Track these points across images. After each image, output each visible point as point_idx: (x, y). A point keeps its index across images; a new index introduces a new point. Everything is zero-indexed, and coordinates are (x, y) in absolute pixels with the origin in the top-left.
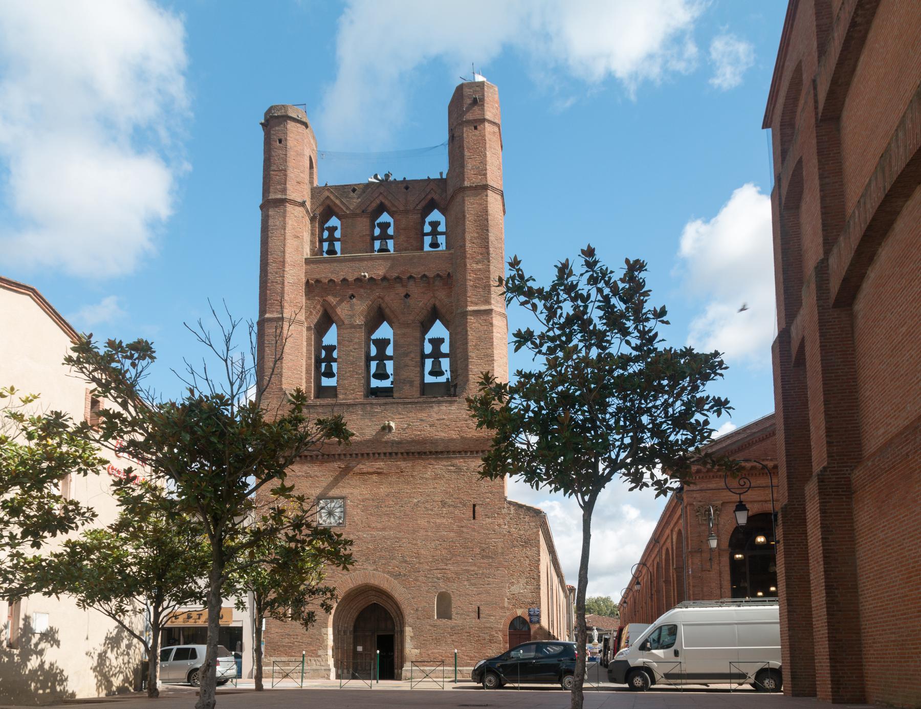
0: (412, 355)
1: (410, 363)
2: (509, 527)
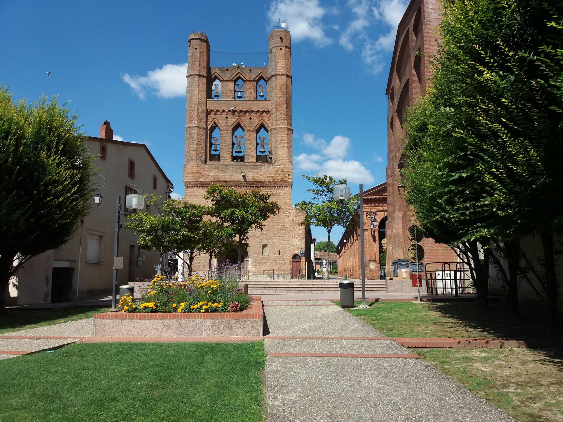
0: (253, 144)
2: (293, 217)
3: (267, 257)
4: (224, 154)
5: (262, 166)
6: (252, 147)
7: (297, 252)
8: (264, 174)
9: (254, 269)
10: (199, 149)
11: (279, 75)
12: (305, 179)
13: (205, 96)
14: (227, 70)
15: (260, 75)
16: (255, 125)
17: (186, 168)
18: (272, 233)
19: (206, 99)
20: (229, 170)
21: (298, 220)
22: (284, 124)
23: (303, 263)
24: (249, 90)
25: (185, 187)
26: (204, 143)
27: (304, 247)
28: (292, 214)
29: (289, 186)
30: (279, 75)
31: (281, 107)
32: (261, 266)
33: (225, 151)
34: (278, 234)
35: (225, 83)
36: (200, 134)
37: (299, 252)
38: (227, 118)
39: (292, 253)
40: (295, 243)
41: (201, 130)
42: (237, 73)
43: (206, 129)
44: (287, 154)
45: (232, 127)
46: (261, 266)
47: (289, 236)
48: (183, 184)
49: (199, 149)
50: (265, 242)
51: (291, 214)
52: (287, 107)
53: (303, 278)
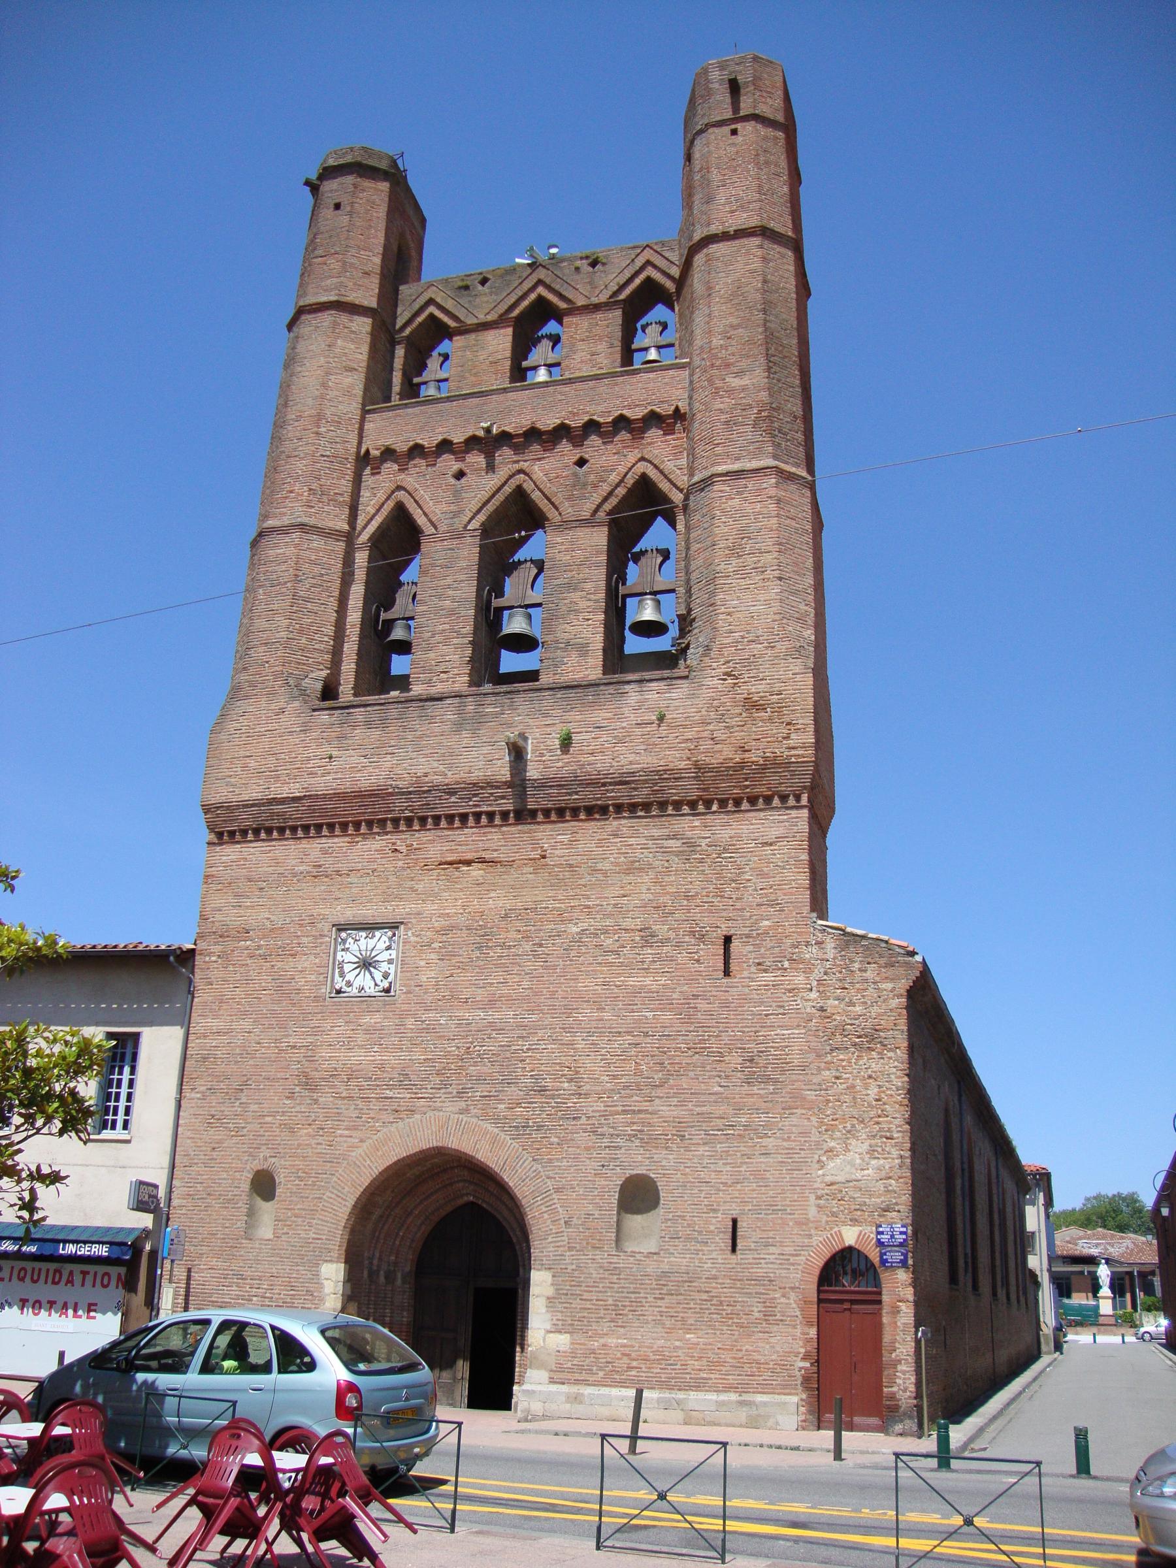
1: (583, 604)
3: (651, 1267)
4: (432, 655)
5: (627, 687)
6: (583, 604)
7: (850, 1236)
8: (638, 731)
9: (562, 1341)
10: (301, 632)
11: (725, 237)
12: (766, 1448)
13: (359, 391)
14: (484, 281)
15: (642, 277)
16: (605, 488)
17: (223, 737)
18: (682, 1103)
19: (364, 405)
20: (436, 728)
21: (858, 1009)
22: (757, 453)
23: (896, 1311)
24: (581, 346)
25: (213, 837)
26: (333, 604)
27: (904, 1200)
28: (817, 973)
29: (798, 798)
30: (725, 237)
31: (740, 374)
32: (605, 1327)
33: (438, 638)
34: (721, 1109)
35: (473, 336)
36: (314, 563)
37: (870, 1231)
38: (460, 475)
39: (815, 1240)
40: (837, 1169)
41: (317, 542)
42: (527, 285)
43: (349, 538)
44: (776, 606)
45: (482, 517)
46: (605, 1327)
47: (794, 1120)
48: (201, 819)
49: (301, 632)
50: (638, 1162)
51: (808, 971)
52: (769, 369)
53: (899, 1427)
